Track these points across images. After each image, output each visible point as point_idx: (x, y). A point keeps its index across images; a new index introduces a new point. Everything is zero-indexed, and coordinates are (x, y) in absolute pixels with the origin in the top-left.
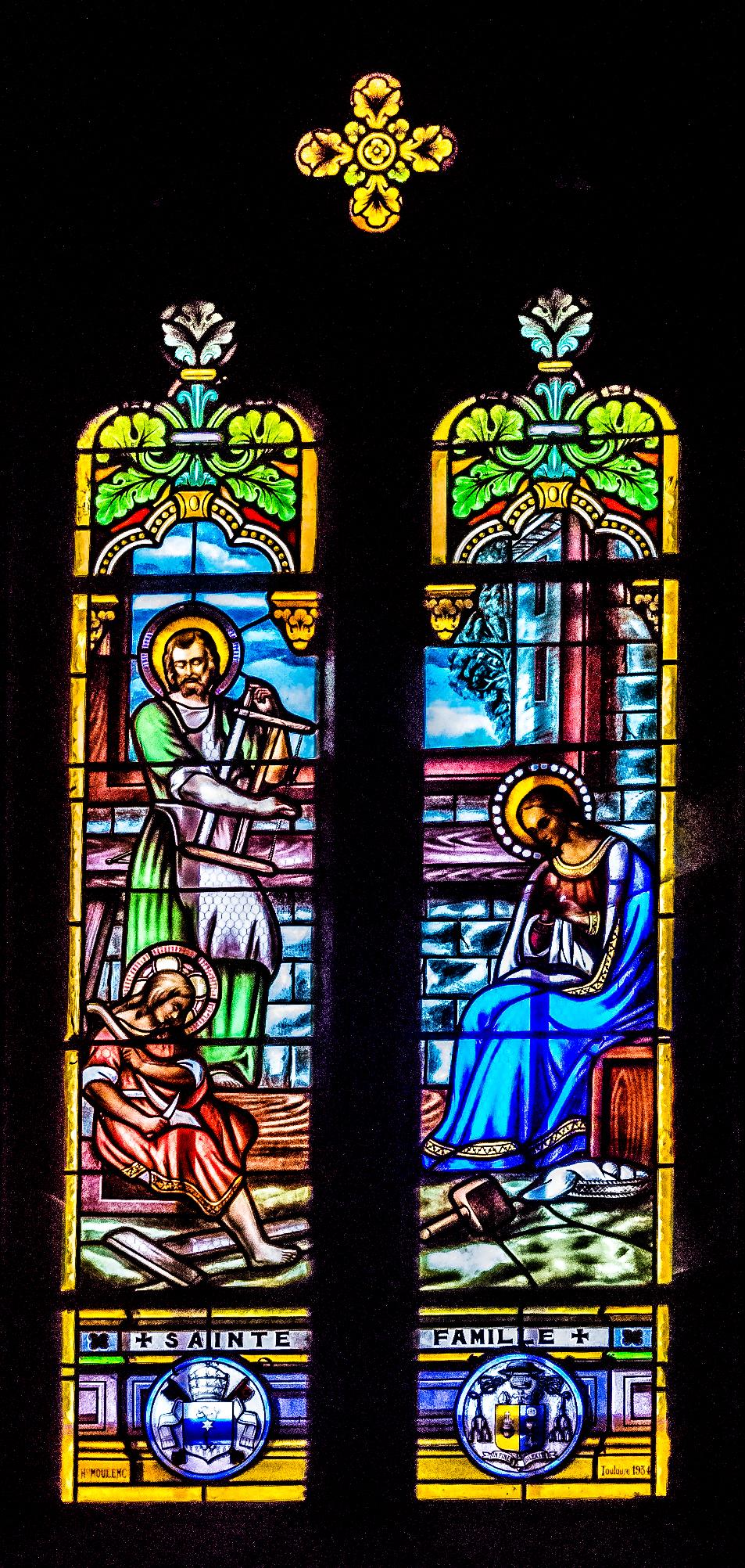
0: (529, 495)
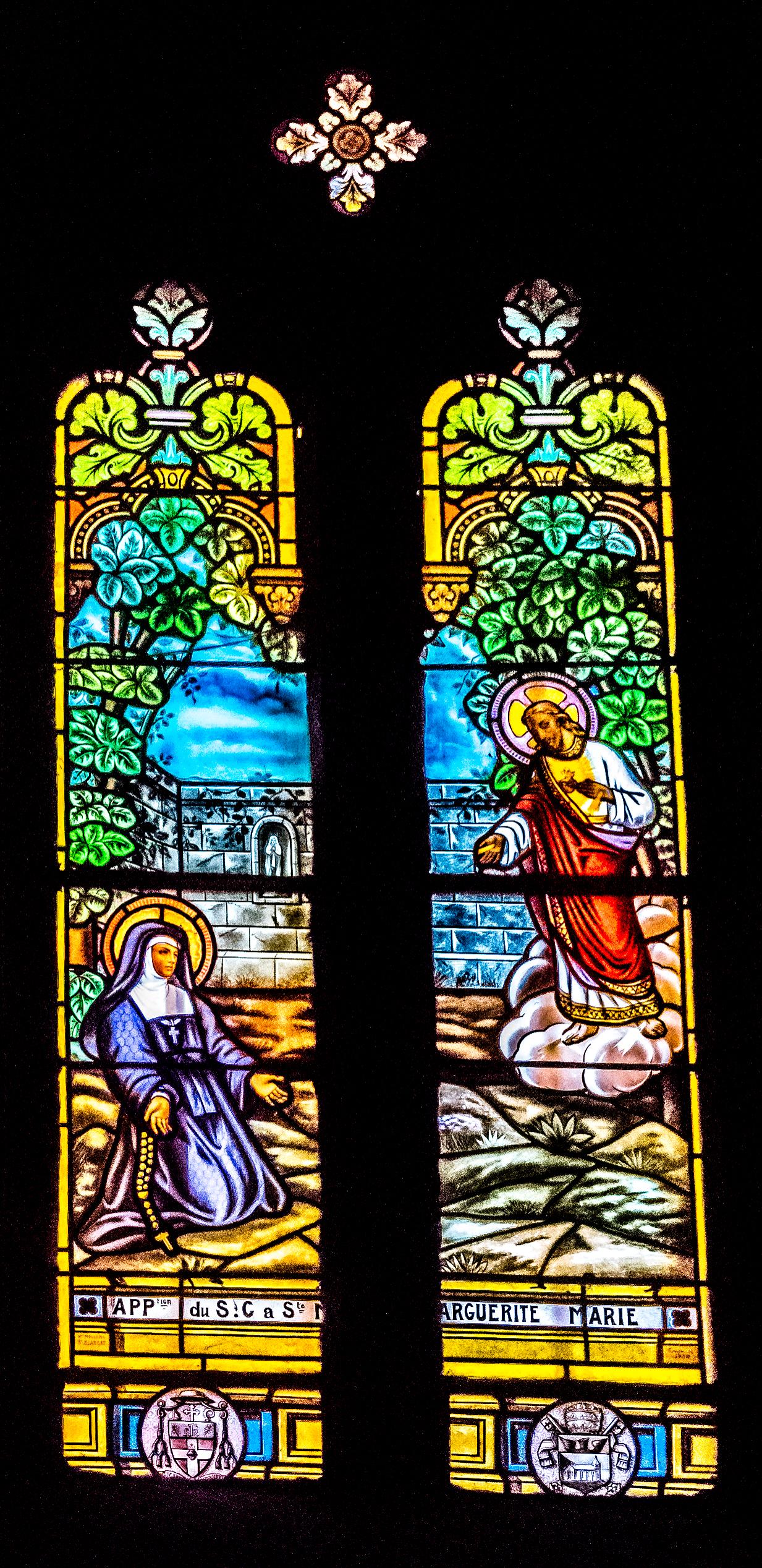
0: (147, 477)
